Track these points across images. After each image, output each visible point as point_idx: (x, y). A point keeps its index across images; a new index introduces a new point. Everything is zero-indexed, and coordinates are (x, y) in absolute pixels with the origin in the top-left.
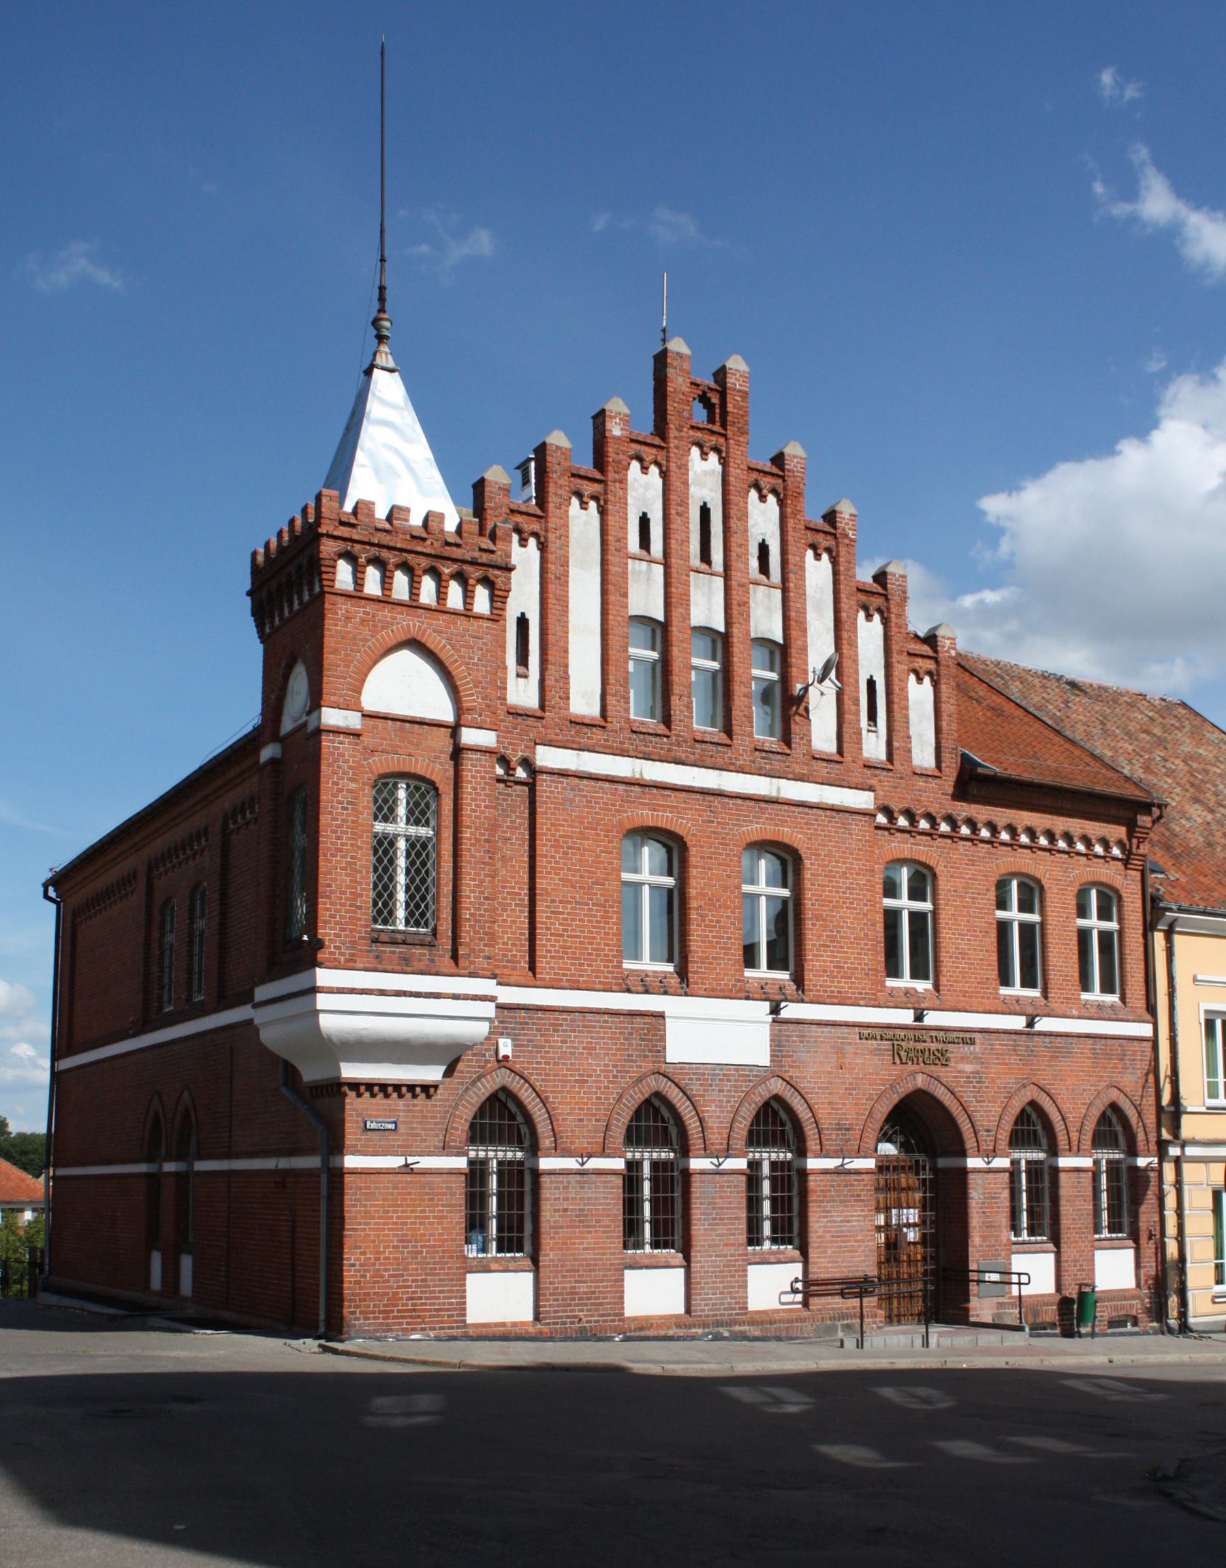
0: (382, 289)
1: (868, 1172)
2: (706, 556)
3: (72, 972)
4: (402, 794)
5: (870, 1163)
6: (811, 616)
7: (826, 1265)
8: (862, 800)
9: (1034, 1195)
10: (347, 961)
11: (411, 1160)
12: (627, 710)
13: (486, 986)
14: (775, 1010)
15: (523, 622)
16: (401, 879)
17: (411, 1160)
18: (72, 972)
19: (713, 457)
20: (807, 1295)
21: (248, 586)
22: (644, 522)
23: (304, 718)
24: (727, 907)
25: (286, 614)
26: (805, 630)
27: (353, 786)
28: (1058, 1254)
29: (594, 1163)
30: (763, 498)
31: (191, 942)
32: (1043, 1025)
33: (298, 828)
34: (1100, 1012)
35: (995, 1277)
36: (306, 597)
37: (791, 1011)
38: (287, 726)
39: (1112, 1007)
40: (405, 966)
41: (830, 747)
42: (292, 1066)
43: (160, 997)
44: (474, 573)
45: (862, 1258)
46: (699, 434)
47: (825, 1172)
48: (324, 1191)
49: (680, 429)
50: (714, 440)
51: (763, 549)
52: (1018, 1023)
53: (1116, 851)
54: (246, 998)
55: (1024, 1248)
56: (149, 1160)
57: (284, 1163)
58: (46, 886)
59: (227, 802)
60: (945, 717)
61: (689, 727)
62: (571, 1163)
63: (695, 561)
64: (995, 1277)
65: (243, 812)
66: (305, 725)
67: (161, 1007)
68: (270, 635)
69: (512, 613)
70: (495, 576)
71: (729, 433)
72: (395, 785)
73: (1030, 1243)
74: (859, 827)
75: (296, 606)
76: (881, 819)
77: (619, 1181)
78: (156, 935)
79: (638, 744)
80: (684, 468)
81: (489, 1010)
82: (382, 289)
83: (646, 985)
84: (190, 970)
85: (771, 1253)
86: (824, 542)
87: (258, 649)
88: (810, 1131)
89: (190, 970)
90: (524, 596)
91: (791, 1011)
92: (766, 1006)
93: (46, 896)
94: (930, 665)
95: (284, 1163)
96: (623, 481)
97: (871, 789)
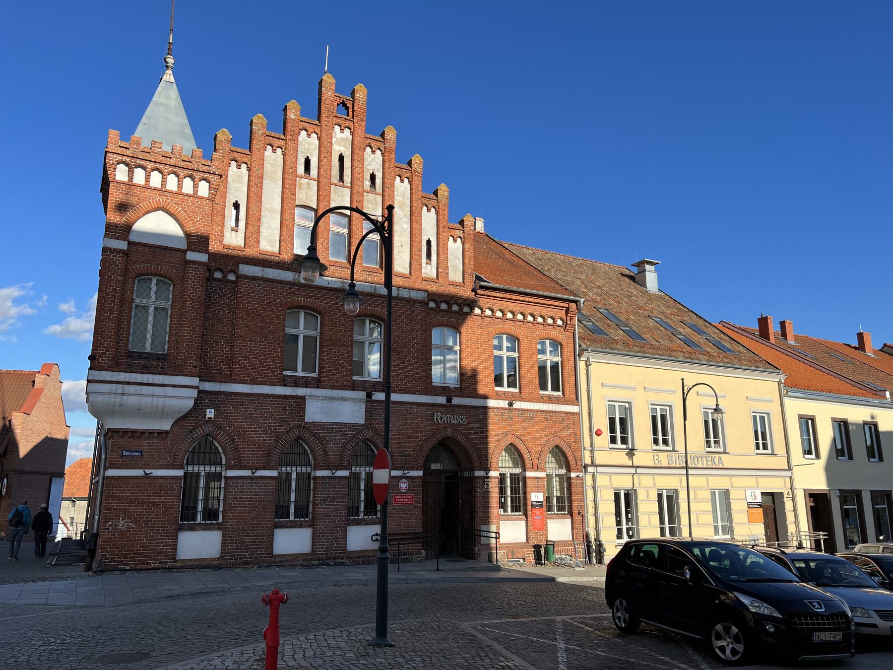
1: (418, 477)
2: (341, 178)
9: (514, 491)
10: (109, 367)
11: (148, 471)
13: (195, 381)
14: (369, 396)
16: (150, 327)
17: (148, 471)
19: (347, 131)
24: (344, 346)
28: (527, 521)
32: (517, 405)
34: (550, 400)
40: (129, 369)
41: (175, 189)
44: (198, 176)
46: (339, 120)
49: (328, 117)
50: (347, 123)
53: (560, 322)
60: (467, 258)
62: (246, 473)
71: (355, 121)
81: (194, 393)
83: (296, 382)
85: (363, 520)
86: (405, 174)
94: (460, 233)
96: (296, 141)
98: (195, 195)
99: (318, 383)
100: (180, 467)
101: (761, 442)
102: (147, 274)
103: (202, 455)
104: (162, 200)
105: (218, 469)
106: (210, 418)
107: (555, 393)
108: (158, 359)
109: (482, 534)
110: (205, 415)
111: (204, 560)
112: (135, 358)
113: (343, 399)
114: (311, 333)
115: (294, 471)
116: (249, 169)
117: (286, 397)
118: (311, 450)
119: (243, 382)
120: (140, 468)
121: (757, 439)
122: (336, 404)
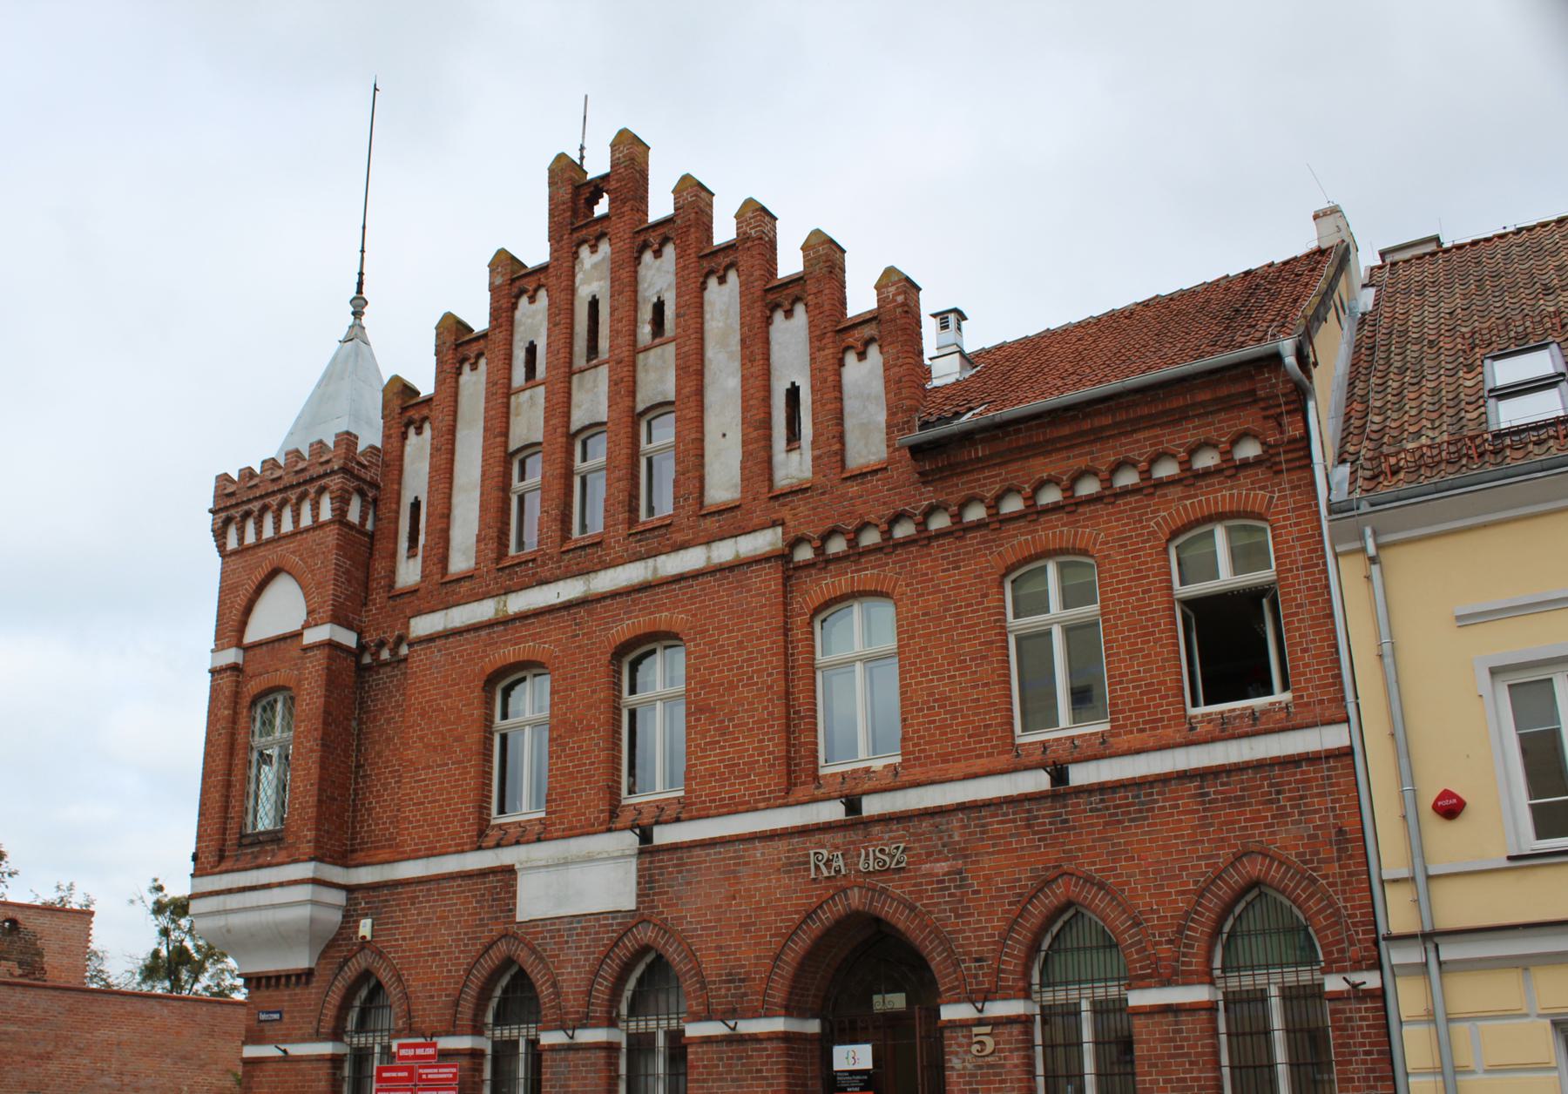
0: (361, 274)
14: (646, 837)
22: (531, 350)
82: (361, 274)
98: (317, 526)
106: (364, 937)
113: (590, 859)
117: (483, 873)
122: (574, 872)
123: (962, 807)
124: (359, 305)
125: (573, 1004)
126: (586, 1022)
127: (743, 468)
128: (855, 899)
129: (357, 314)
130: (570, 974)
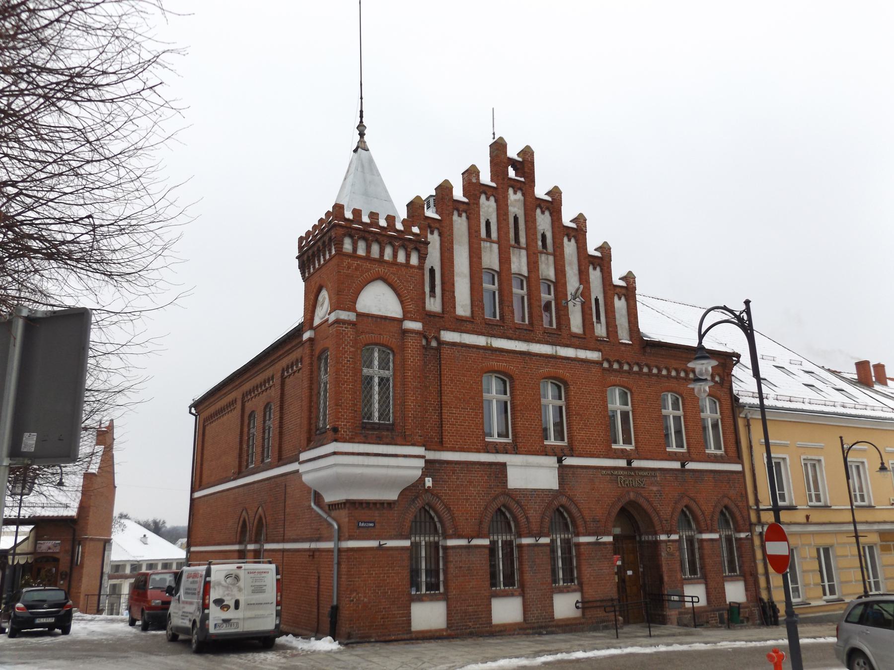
0: (361, 112)
1: (609, 543)
3: (203, 449)
4: (376, 354)
5: (610, 539)
6: (567, 268)
7: (593, 593)
8: (594, 356)
11: (382, 542)
12: (483, 314)
13: (420, 451)
14: (560, 461)
15: (432, 271)
17: (382, 542)
18: (203, 449)
20: (584, 608)
21: (297, 254)
22: (488, 224)
23: (327, 316)
25: (317, 266)
26: (565, 275)
27: (352, 349)
29: (476, 542)
30: (543, 212)
31: (264, 432)
33: (322, 372)
35: (676, 598)
36: (327, 257)
37: (569, 461)
38: (317, 321)
39: (721, 456)
40: (379, 441)
42: (319, 493)
43: (247, 460)
45: (608, 588)
47: (589, 544)
48: (336, 561)
51: (544, 237)
52: (676, 465)
54: (296, 459)
55: (690, 581)
56: (240, 543)
57: (313, 545)
58: (190, 407)
59: (284, 362)
61: (513, 321)
62: (463, 542)
63: (513, 242)
64: (676, 598)
65: (292, 367)
66: (327, 320)
67: (247, 466)
68: (308, 277)
69: (427, 266)
70: (420, 245)
72: (373, 349)
73: (691, 579)
74: (595, 369)
75: (322, 262)
76: (606, 365)
77: (487, 551)
78: (246, 429)
79: (490, 329)
80: (506, 198)
81: (421, 463)
82: (361, 112)
84: (263, 447)
87: (302, 284)
88: (580, 522)
89: (263, 447)
90: (434, 258)
91: (569, 461)
92: (555, 459)
93: (190, 412)
95: (313, 545)
97: (599, 350)
99: (514, 449)
100: (407, 537)
101: (813, 493)
102: (372, 344)
103: (423, 524)
104: (381, 270)
105: (436, 539)
106: (429, 487)
107: (628, 447)
108: (388, 430)
109: (666, 598)
110: (424, 484)
111: (430, 631)
112: (368, 429)
113: (540, 466)
114: (677, 413)
115: (423, 540)
116: (440, 235)
118: (439, 517)
119: (453, 450)
120: (374, 539)
121: (809, 490)
123: (660, 469)
124: (361, 129)
125: (535, 527)
126: (541, 535)
127: (569, 319)
128: (632, 495)
129: (362, 135)
130: (534, 513)
